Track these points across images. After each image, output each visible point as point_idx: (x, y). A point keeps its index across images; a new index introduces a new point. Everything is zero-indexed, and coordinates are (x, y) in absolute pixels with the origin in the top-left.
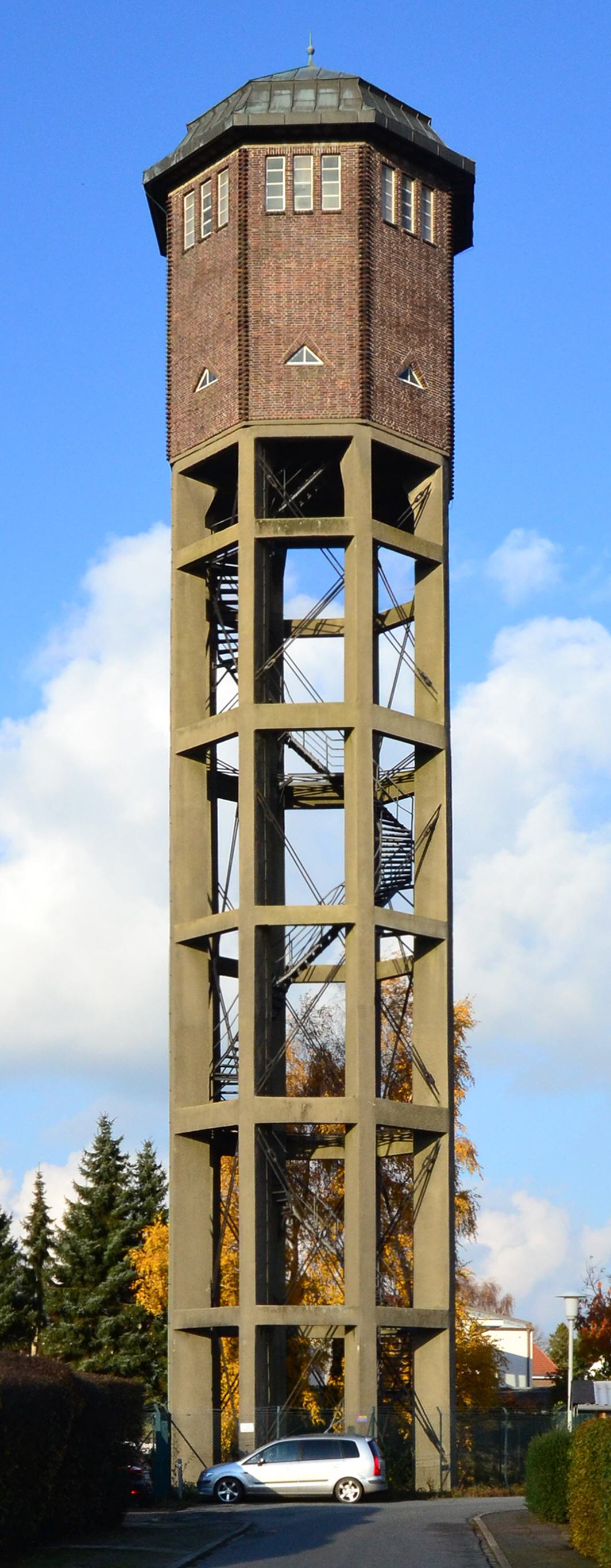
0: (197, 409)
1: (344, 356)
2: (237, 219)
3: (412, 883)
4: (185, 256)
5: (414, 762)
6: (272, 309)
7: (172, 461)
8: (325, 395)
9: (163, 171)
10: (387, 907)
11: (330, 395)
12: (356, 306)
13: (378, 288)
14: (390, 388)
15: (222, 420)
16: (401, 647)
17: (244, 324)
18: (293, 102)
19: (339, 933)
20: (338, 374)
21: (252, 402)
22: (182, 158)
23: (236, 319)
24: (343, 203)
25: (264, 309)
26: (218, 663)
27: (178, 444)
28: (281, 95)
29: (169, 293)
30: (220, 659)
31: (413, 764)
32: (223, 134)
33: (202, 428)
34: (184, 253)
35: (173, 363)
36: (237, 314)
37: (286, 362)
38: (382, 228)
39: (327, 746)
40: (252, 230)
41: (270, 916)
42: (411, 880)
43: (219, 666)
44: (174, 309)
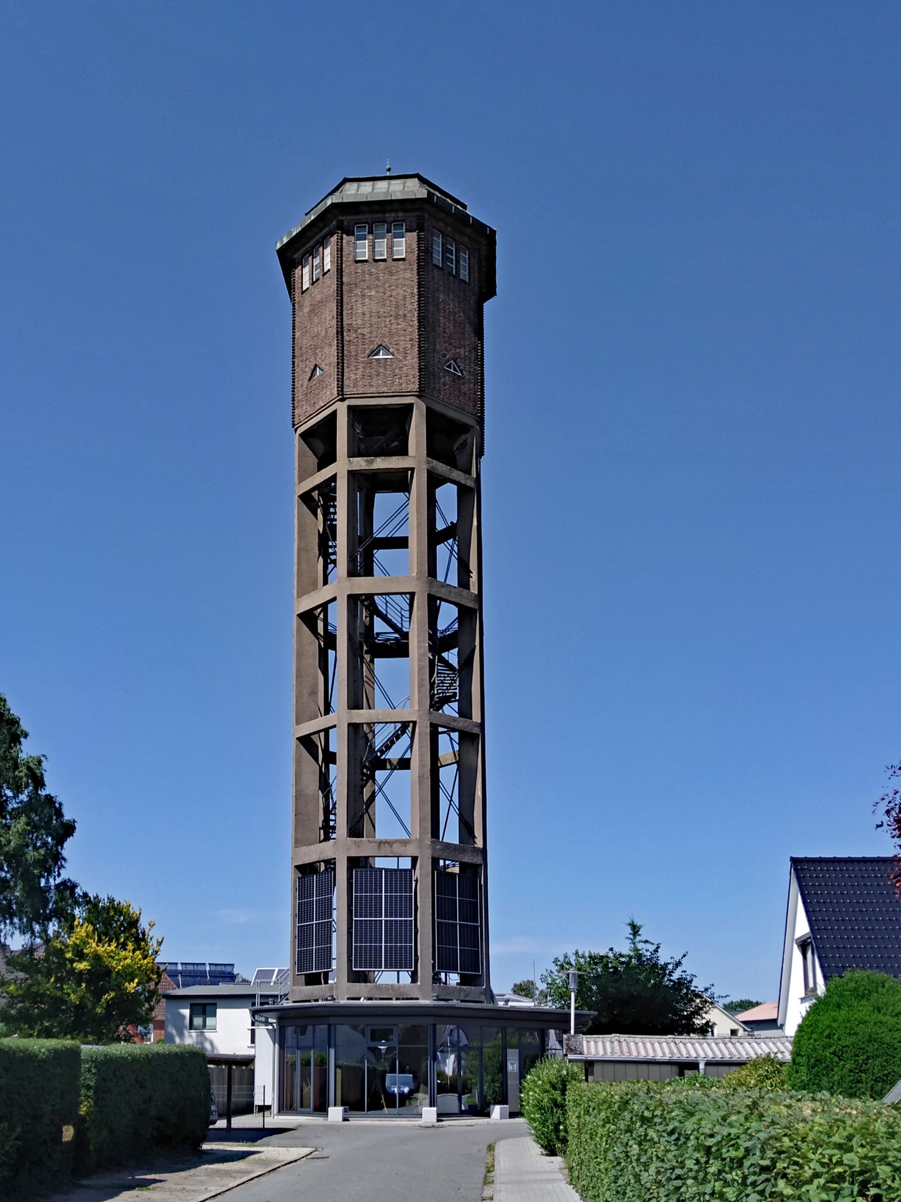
0: (311, 392)
1: (408, 352)
2: (336, 265)
3: (457, 698)
4: (304, 295)
5: (457, 624)
6: (360, 322)
7: (296, 427)
8: (395, 377)
9: (288, 240)
10: (440, 711)
11: (398, 377)
12: (415, 319)
13: (467, 999)
14: (439, 373)
15: (327, 396)
16: (451, 546)
17: (340, 332)
18: (373, 189)
19: (407, 731)
20: (404, 363)
21: (346, 382)
22: (300, 229)
23: (335, 331)
24: (406, 252)
25: (354, 322)
26: (329, 561)
27: (299, 416)
28: (366, 185)
29: (293, 376)
30: (330, 559)
31: (456, 626)
32: (326, 209)
33: (314, 403)
34: (303, 292)
35: (296, 364)
36: (335, 326)
37: (368, 357)
38: (433, 269)
39: (402, 615)
40: (346, 271)
41: (361, 716)
42: (456, 696)
43: (330, 563)
44: (296, 330)
